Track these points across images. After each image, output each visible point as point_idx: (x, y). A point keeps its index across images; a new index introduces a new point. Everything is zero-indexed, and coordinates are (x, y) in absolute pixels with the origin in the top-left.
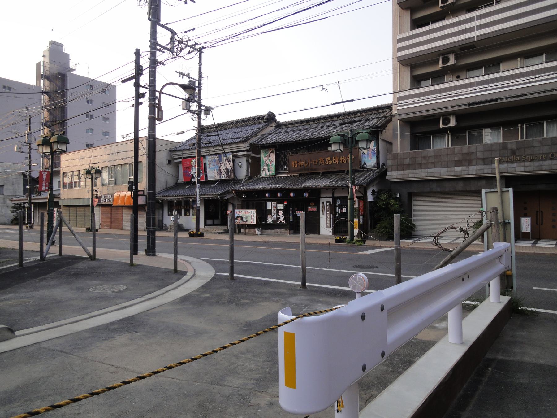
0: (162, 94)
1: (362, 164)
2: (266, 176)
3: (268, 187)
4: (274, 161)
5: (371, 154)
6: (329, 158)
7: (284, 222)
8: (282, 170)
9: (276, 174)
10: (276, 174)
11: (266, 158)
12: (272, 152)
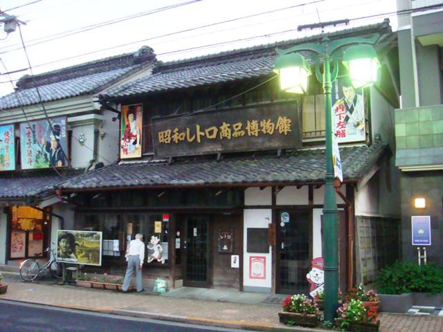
6: (240, 125)
7: (198, 127)
12: (140, 105)
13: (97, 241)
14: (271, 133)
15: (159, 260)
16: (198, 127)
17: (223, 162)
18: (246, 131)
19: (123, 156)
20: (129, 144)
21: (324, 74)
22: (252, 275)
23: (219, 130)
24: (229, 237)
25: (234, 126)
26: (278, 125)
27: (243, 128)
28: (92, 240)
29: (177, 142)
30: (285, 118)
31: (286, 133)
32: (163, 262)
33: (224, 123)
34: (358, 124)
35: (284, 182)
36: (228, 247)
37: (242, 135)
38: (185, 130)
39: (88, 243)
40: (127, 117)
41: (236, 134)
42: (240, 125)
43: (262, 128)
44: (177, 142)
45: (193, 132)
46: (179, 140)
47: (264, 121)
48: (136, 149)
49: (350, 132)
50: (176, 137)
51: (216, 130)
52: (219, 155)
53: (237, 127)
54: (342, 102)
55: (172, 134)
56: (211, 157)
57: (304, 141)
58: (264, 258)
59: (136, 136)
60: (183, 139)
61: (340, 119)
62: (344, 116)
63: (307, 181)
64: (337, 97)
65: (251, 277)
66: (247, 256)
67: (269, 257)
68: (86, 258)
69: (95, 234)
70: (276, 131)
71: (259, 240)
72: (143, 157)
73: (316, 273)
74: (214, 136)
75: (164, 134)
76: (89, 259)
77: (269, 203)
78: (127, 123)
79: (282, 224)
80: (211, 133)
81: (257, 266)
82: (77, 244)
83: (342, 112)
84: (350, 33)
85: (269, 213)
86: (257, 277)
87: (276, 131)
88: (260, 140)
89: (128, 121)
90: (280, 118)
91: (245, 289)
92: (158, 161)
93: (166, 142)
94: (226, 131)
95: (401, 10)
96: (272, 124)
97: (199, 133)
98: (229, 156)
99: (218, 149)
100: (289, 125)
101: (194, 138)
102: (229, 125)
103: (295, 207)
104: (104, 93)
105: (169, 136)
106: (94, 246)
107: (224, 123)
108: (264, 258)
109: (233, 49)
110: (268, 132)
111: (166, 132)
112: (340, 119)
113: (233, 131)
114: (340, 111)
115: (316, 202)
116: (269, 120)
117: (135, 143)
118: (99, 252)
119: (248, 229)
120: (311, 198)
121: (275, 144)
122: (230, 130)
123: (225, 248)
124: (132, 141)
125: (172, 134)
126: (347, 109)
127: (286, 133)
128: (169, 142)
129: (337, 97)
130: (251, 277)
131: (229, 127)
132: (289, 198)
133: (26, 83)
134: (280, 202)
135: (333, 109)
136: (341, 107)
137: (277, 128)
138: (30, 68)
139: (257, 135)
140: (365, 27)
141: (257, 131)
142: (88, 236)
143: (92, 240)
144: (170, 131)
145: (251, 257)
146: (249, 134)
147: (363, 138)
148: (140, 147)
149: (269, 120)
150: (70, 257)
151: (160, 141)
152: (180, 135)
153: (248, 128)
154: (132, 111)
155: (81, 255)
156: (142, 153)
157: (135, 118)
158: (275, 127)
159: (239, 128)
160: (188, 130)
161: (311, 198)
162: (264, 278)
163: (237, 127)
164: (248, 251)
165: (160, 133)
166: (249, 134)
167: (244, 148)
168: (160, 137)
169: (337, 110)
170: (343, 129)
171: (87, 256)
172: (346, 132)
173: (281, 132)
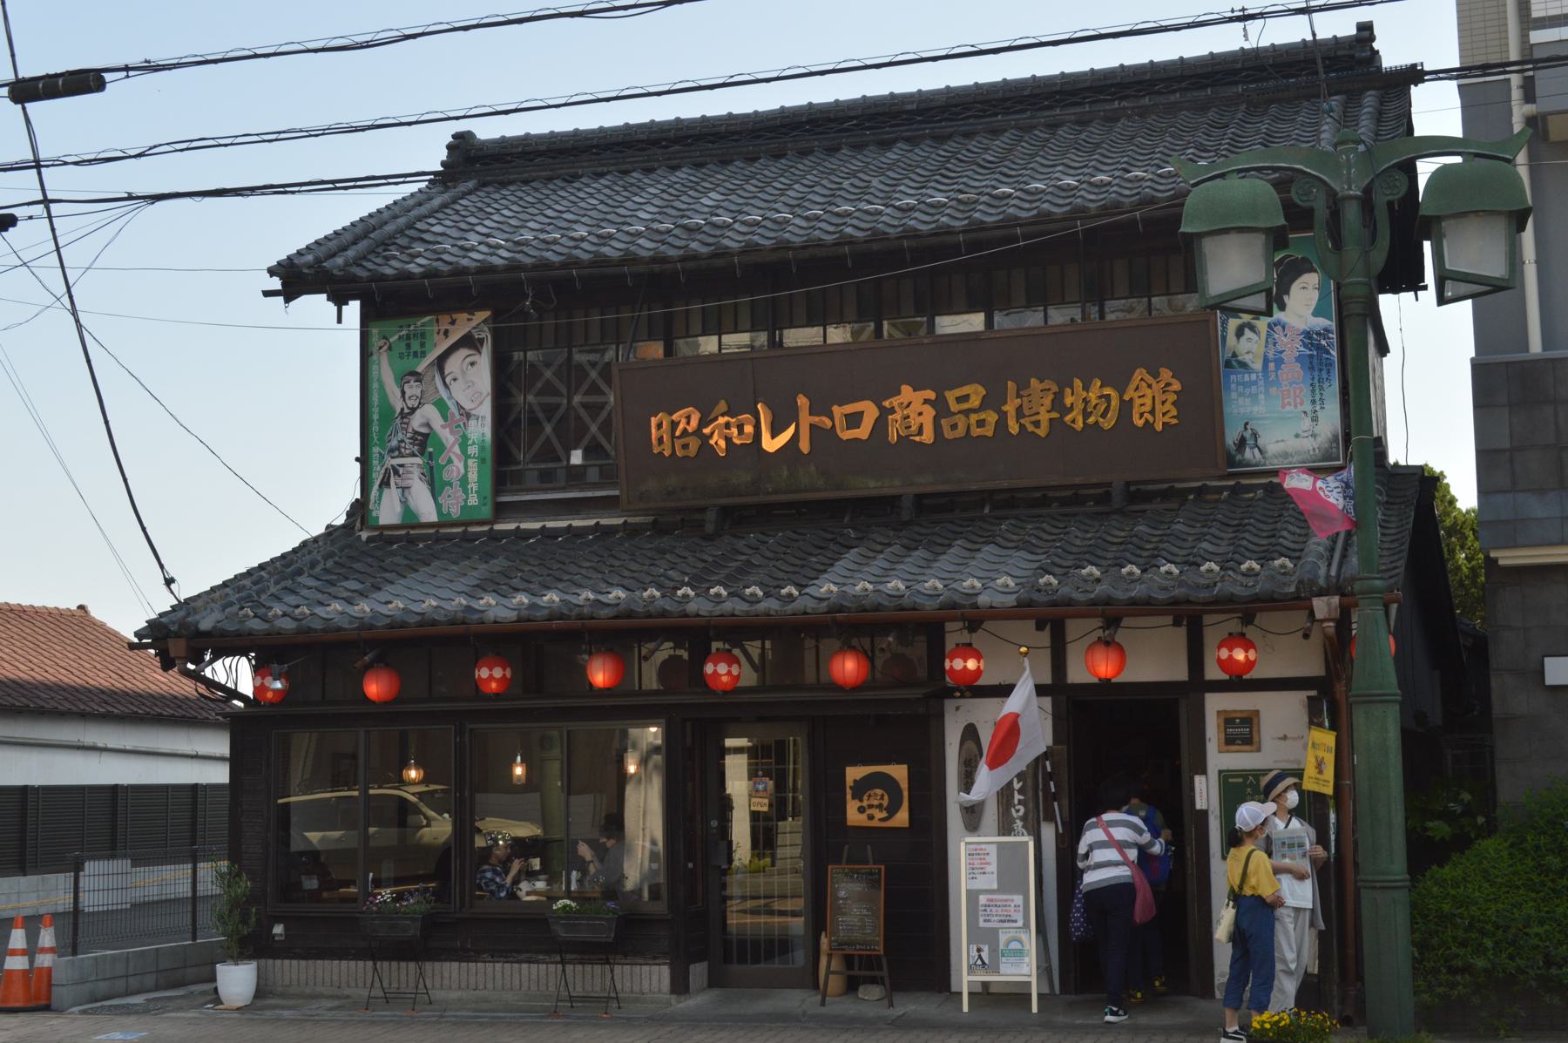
0: (40, 197)
1: (1231, 438)
2: (410, 522)
3: (496, 608)
4: (486, 410)
5: (1293, 371)
6: (976, 393)
7: (802, 401)
8: (547, 478)
9: (501, 510)
10: (501, 510)
11: (413, 389)
12: (469, 342)
25: (951, 396)
33: (906, 389)
42: (976, 393)
47: (1078, 383)
51: (870, 411)
74: (863, 432)
80: (854, 420)
84: (1235, 72)
95: (1479, 61)
96: (1107, 391)
122: (930, 413)
127: (1159, 427)
133: (471, 163)
138: (37, 165)
140: (559, 134)
141: (1044, 417)
159: (975, 402)
164: (1029, 983)
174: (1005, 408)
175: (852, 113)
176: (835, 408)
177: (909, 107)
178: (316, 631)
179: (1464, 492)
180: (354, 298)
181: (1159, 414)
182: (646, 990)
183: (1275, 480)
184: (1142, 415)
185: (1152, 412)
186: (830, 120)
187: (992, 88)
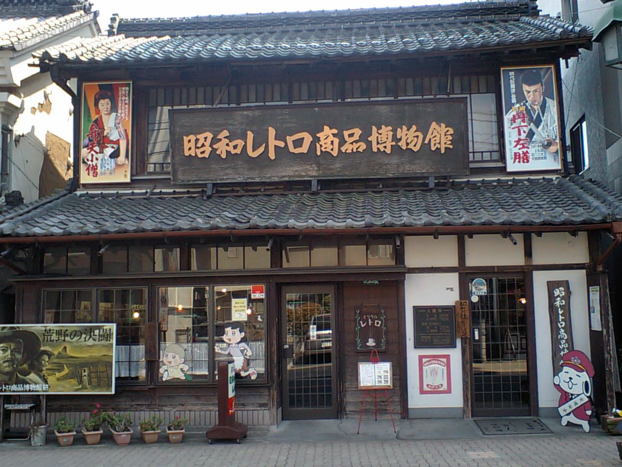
6: (357, 132)
7: (272, 132)
13: (104, 342)
14: (416, 149)
15: (243, 374)
16: (272, 132)
17: (323, 194)
18: (369, 144)
19: (86, 178)
20: (100, 156)
21: (221, 95)
22: (425, 388)
23: (316, 140)
24: (378, 324)
25: (346, 133)
26: (429, 136)
27: (364, 138)
28: (91, 342)
29: (224, 156)
30: (443, 125)
31: (443, 151)
32: (254, 377)
33: (326, 128)
34: (549, 144)
35: (544, 223)
36: (378, 342)
37: (361, 150)
38: (244, 137)
39: (81, 348)
40: (96, 104)
41: (348, 148)
42: (357, 132)
43: (400, 139)
44: (224, 156)
45: (261, 140)
46: (228, 152)
47: (405, 128)
48: (118, 166)
49: (536, 155)
50: (222, 148)
51: (308, 138)
52: (314, 183)
53: (351, 135)
54: (523, 108)
55: (215, 140)
56: (290, 186)
57: (472, 165)
58: (447, 357)
59: (117, 142)
60: (238, 151)
61: (520, 134)
62: (526, 130)
63: (584, 222)
64: (514, 100)
65: (422, 392)
66: (413, 355)
67: (456, 355)
68: (74, 381)
69: (99, 328)
70: (425, 146)
71: (436, 326)
72: (133, 183)
73: (569, 375)
74: (304, 149)
75: (197, 140)
76: (81, 382)
77: (455, 263)
78: (94, 117)
79: (475, 299)
80: (298, 143)
81: (434, 372)
82: (45, 352)
83: (523, 124)
85: (453, 279)
86: (435, 391)
87: (425, 146)
88: (395, 160)
89: (98, 112)
90: (434, 125)
91: (411, 415)
92: (171, 191)
93: (200, 156)
94: (329, 141)
97: (273, 142)
98: (330, 186)
99: (311, 172)
100: (450, 138)
101: (261, 150)
102: (335, 131)
103: (502, 270)
104: (54, 51)
105: (208, 143)
106: (96, 353)
107: (326, 128)
108: (447, 357)
109: (207, 15)
110: (411, 146)
111: (201, 137)
112: (520, 134)
113: (342, 142)
114: (518, 121)
115: (537, 260)
116: (414, 128)
117: (115, 155)
118: (110, 364)
119: (416, 309)
120: (528, 253)
121: (419, 168)
122: (336, 141)
123: (371, 343)
124: (109, 151)
125: (215, 140)
126: (531, 119)
127: (443, 151)
128: (206, 155)
129: (514, 100)
130: (422, 392)
131: (334, 135)
132: (490, 253)
134: (472, 261)
135: (507, 118)
136: (520, 115)
137: (426, 142)
139: (388, 151)
141: (389, 144)
142: (76, 333)
143: (91, 342)
144: (210, 136)
145: (421, 358)
146: (375, 150)
147: (558, 166)
148: (128, 163)
149: (414, 128)
150: (25, 382)
151: (187, 153)
152: (232, 144)
153: (373, 138)
154: (109, 93)
155: (58, 375)
156: (132, 175)
157: (114, 108)
158: (424, 139)
160: (250, 135)
161: (528, 253)
162: (449, 391)
163: (351, 135)
164: (418, 345)
165: (186, 139)
166: (375, 150)
167: (362, 172)
168: (186, 145)
169: (514, 120)
170: (525, 150)
171: (75, 375)
172: (530, 155)
173: (433, 148)
174: (369, 139)
175: (307, 16)
176: (288, 137)
177: (333, 15)
178: (74, 234)
179: (32, 405)
180: (74, 77)
181: (442, 143)
182: (256, 423)
183: (427, 181)
184: (435, 145)
185: (440, 143)
186: (296, 19)
187: (588, 144)
